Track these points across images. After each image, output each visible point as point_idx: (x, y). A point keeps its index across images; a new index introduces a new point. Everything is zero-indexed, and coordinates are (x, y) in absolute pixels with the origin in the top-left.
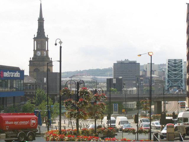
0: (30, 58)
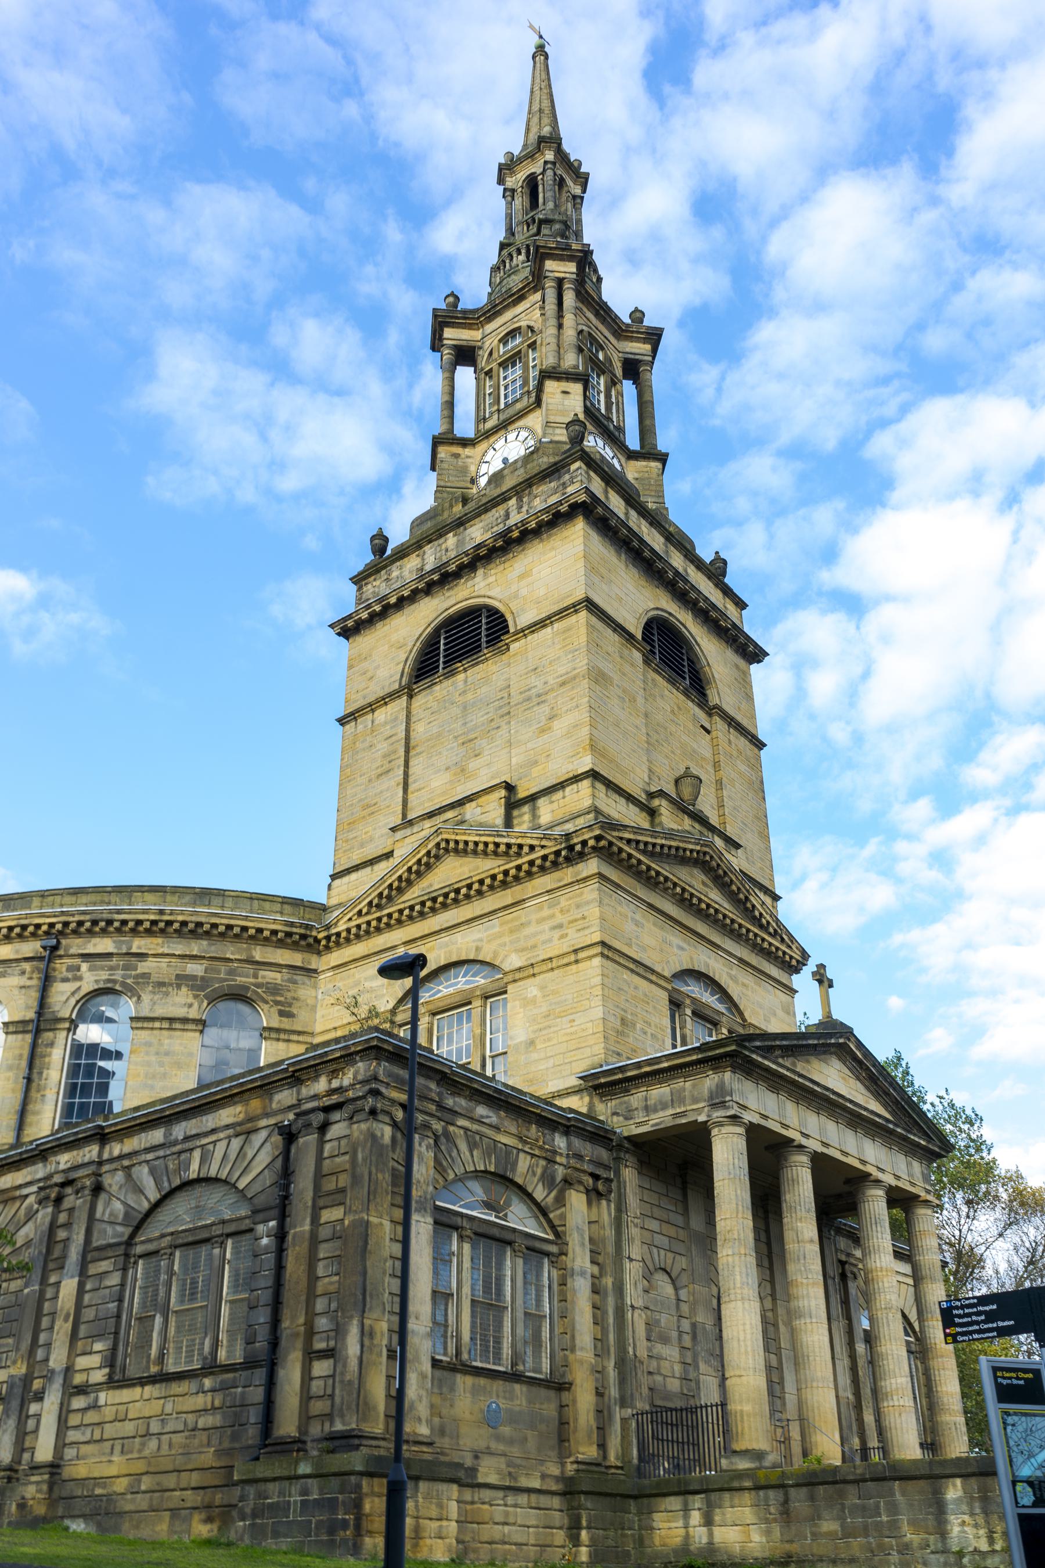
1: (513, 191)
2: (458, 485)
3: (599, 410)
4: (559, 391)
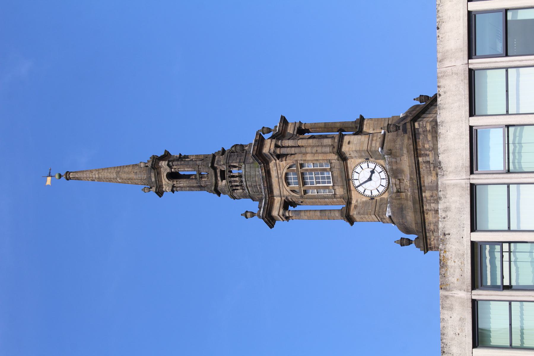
0: (405, 242)
2: (374, 205)
4: (348, 146)
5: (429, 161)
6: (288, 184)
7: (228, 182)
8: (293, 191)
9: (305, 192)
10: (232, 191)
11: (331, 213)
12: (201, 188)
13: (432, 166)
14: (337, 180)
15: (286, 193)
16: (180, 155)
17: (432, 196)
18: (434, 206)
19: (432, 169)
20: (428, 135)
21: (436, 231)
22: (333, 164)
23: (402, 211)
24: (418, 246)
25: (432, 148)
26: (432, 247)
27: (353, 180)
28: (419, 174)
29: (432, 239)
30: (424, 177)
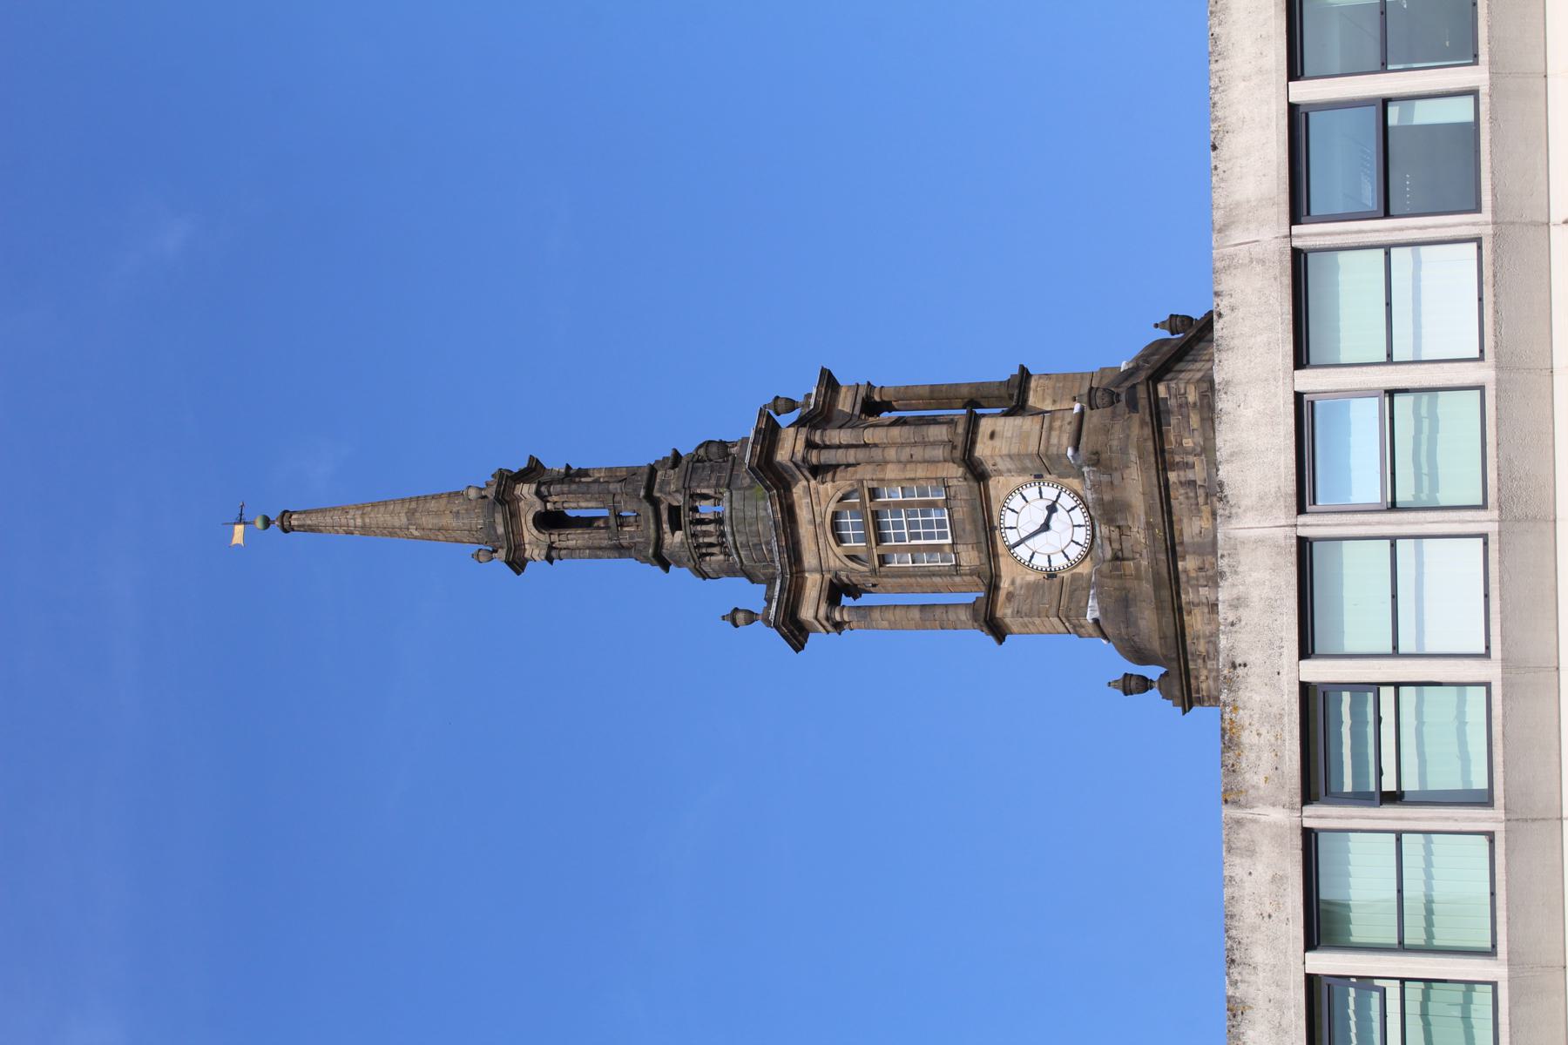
0: (1133, 685)
1: (551, 547)
2: (1057, 592)
3: (1181, 338)
4: (989, 442)
5: (1195, 482)
6: (840, 540)
7: (689, 536)
8: (852, 558)
9: (883, 560)
10: (699, 558)
11: (947, 612)
12: (620, 550)
13: (1201, 492)
14: (964, 530)
15: (834, 563)
16: (568, 467)
17: (1201, 569)
18: (1207, 593)
19: (1201, 500)
20: (1192, 415)
21: (1212, 656)
22: (952, 490)
23: (1127, 607)
24: (1166, 695)
25: (1201, 447)
26: (1203, 696)
27: (1003, 530)
28: (1170, 513)
29: (1203, 678)
30: (1181, 520)
